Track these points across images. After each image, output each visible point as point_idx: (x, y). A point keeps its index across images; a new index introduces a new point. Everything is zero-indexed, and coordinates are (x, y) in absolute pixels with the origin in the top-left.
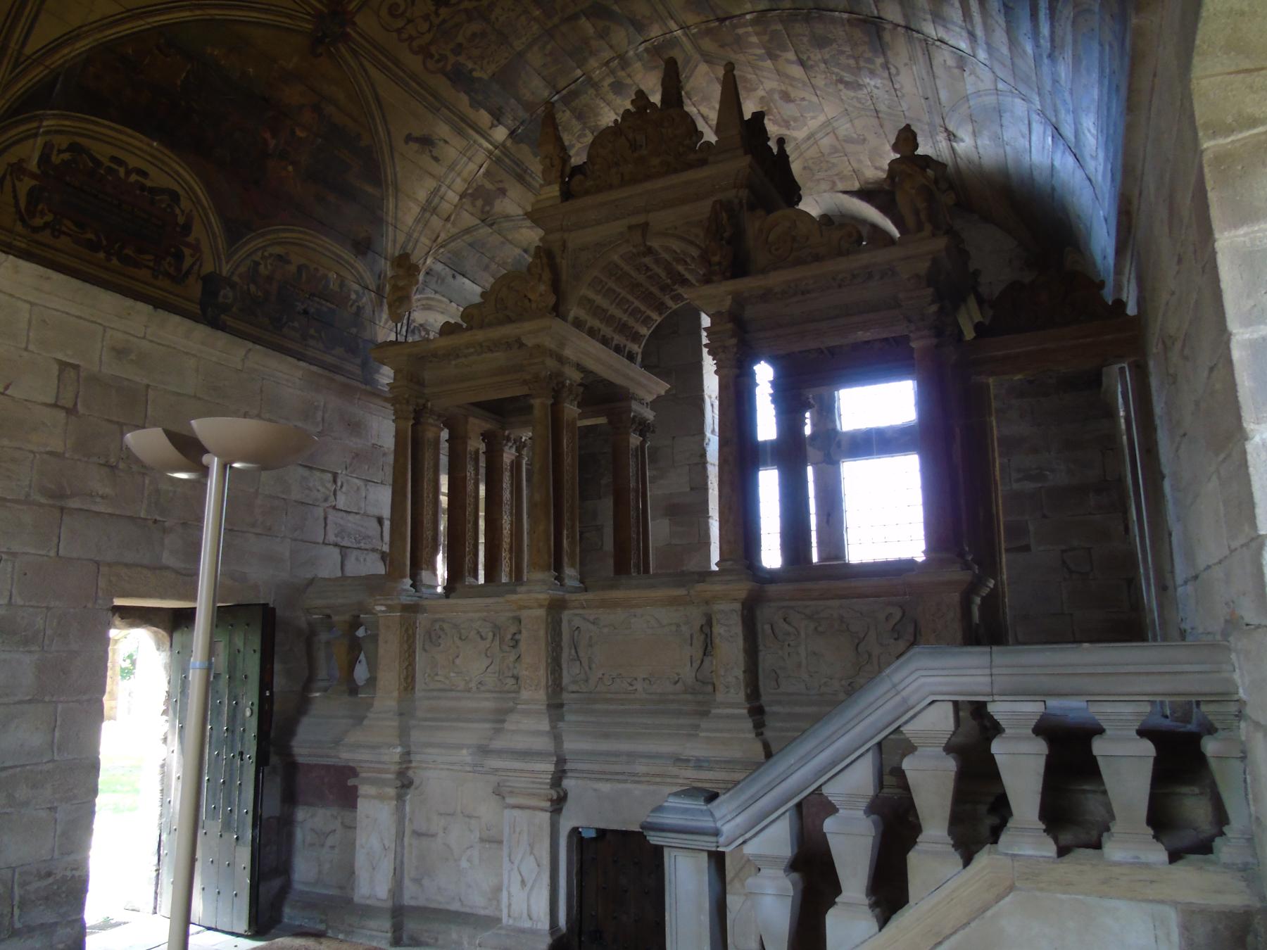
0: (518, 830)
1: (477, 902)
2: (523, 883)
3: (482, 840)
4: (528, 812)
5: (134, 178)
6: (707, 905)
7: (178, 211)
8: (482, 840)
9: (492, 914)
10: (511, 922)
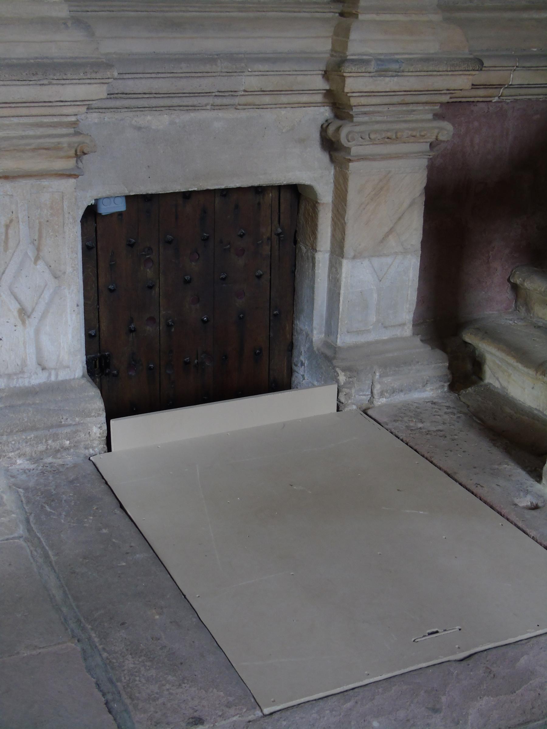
2: (24, 314)
4: (26, 184)
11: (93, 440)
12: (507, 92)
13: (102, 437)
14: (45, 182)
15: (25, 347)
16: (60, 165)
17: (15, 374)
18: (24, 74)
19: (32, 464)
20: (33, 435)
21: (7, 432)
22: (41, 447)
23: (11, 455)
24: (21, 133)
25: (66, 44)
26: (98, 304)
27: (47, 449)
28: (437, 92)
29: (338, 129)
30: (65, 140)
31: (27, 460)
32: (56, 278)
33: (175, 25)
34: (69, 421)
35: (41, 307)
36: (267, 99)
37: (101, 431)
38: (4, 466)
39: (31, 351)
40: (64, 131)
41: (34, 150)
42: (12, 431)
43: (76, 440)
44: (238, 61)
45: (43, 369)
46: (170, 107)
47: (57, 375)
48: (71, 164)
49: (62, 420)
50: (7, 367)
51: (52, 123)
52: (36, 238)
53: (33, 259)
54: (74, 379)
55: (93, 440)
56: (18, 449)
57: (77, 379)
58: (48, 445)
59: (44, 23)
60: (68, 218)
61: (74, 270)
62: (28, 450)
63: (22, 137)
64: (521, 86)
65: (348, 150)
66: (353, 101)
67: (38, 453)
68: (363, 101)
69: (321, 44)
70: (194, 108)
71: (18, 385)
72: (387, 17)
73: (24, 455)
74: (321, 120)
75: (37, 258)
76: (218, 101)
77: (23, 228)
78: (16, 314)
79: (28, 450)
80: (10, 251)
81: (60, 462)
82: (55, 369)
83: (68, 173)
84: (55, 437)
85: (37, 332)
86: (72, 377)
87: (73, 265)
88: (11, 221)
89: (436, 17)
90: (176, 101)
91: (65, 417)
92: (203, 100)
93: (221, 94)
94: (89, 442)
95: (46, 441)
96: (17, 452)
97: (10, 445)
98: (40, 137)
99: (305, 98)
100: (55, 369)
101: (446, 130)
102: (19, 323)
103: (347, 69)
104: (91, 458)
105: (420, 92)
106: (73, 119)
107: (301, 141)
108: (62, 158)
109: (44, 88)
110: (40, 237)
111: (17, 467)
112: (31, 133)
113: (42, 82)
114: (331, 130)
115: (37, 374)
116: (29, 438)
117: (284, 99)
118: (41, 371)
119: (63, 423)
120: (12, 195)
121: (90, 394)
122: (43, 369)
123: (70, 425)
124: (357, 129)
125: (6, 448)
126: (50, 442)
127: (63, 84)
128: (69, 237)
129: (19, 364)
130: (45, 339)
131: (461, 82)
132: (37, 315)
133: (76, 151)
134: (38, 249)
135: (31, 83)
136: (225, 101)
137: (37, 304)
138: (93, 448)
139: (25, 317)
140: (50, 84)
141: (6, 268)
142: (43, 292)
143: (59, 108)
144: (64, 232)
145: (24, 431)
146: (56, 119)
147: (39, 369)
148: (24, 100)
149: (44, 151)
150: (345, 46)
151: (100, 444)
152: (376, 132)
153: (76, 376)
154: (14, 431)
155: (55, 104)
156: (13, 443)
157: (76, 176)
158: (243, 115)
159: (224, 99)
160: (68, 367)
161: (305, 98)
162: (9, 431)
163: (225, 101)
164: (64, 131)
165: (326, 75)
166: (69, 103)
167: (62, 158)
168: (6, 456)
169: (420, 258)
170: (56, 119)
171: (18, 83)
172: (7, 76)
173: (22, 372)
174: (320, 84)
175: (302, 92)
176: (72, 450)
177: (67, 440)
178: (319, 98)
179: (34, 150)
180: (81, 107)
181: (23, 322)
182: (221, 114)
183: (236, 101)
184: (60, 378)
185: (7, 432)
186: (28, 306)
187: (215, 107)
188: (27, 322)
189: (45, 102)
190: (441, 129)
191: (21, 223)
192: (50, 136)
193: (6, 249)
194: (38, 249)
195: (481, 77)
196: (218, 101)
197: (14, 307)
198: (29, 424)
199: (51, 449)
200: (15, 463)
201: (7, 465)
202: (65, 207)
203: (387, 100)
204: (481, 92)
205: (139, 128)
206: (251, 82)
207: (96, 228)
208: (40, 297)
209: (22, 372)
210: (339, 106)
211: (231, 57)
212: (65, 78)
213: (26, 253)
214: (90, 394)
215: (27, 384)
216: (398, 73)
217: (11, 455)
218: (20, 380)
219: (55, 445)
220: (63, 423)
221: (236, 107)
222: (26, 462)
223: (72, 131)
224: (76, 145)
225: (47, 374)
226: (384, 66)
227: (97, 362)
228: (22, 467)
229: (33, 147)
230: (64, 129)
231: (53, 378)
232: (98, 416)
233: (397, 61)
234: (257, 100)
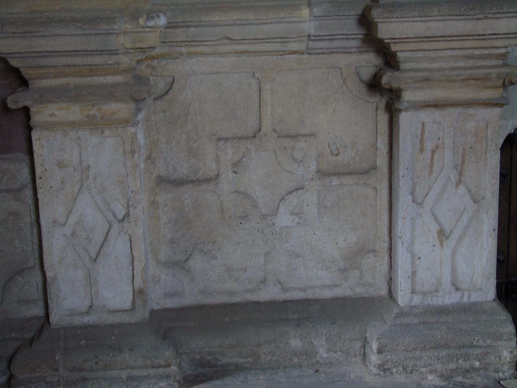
0: (429, 145)
1: (315, 277)
2: (442, 235)
3: (322, 174)
4: (455, 111)
6: (401, 140)
8: (322, 174)
9: (349, 293)
10: (417, 300)
11: (503, 364)
13: (513, 362)
14: (472, 111)
15: (441, 267)
16: (486, 94)
17: (430, 292)
18: (462, 9)
19: (442, 381)
20: (445, 353)
21: (420, 347)
22: (452, 366)
23: (423, 370)
24: (452, 64)
26: (509, 230)
27: (457, 368)
30: (494, 71)
31: (438, 377)
32: (475, 202)
34: (481, 343)
35: (459, 230)
37: (512, 356)
38: (416, 381)
39: (447, 271)
40: (493, 62)
42: (425, 347)
43: (486, 362)
45: (457, 289)
47: (469, 297)
48: (497, 93)
49: (474, 341)
50: (423, 285)
51: (483, 55)
52: (459, 163)
53: (455, 183)
54: (486, 302)
55: (503, 364)
56: (430, 365)
57: (489, 302)
58: (458, 364)
60: (491, 145)
61: (493, 195)
62: (439, 367)
63: (454, 69)
67: (448, 371)
71: (431, 303)
73: (435, 371)
75: (459, 183)
77: (448, 154)
78: (435, 234)
79: (439, 367)
80: (435, 175)
81: (470, 382)
82: (468, 290)
83: (494, 102)
84: (466, 357)
85: (454, 253)
86: (484, 300)
87: (493, 191)
88: (437, 147)
91: (476, 339)
94: (499, 366)
95: (457, 360)
96: (428, 368)
97: (423, 360)
98: (470, 68)
100: (468, 290)
102: (437, 243)
104: (501, 382)
106: (503, 51)
108: (489, 88)
109: (480, 22)
110: (463, 163)
111: (428, 383)
112: (462, 64)
113: (478, 16)
115: (451, 294)
116: (441, 355)
118: (454, 291)
119: (475, 344)
120: (440, 123)
121: (502, 317)
122: (457, 289)
123: (481, 347)
125: (418, 363)
126: (461, 361)
127: (498, 18)
128: (491, 164)
129: (435, 283)
130: (460, 262)
132: (455, 236)
133: (504, 81)
134: (460, 174)
135: (468, 17)
137: (455, 226)
138: (503, 373)
139: (444, 238)
140: (485, 18)
141: (429, 191)
142: (462, 215)
143: (491, 41)
144: (486, 159)
145: (437, 347)
146: (486, 52)
147: (453, 290)
148: (460, 34)
149: (473, 82)
151: (510, 369)
153: (488, 299)
154: (428, 347)
155: (487, 37)
156: (426, 358)
157: (501, 105)
160: (481, 289)
162: (422, 346)
164: (493, 62)
166: (501, 36)
167: (489, 88)
168: (418, 370)
169: (499, 155)
170: (486, 52)
171: (455, 17)
172: (446, 11)
173: (437, 291)
176: (482, 372)
177: (477, 361)
180: (512, 39)
181: (442, 243)
184: (472, 300)
185: (420, 347)
186: (447, 228)
188: (445, 243)
189: (479, 35)
191: (446, 149)
192: (479, 67)
193: (431, 173)
194: (460, 174)
197: (434, 228)
198: (442, 342)
199: (461, 368)
200: (426, 378)
201: (418, 380)
202: (489, 134)
207: (511, 157)
208: (459, 220)
209: (437, 291)
212: (501, 11)
213: (449, 177)
214: (502, 317)
215: (440, 303)
217: (423, 370)
218: (434, 299)
219: (466, 365)
220: (475, 344)
222: (437, 379)
223: (500, 62)
224: (504, 76)
225: (460, 295)
227: (504, 287)
228: (433, 383)
229: (463, 77)
230: (493, 61)
231: (465, 299)
232: (509, 340)
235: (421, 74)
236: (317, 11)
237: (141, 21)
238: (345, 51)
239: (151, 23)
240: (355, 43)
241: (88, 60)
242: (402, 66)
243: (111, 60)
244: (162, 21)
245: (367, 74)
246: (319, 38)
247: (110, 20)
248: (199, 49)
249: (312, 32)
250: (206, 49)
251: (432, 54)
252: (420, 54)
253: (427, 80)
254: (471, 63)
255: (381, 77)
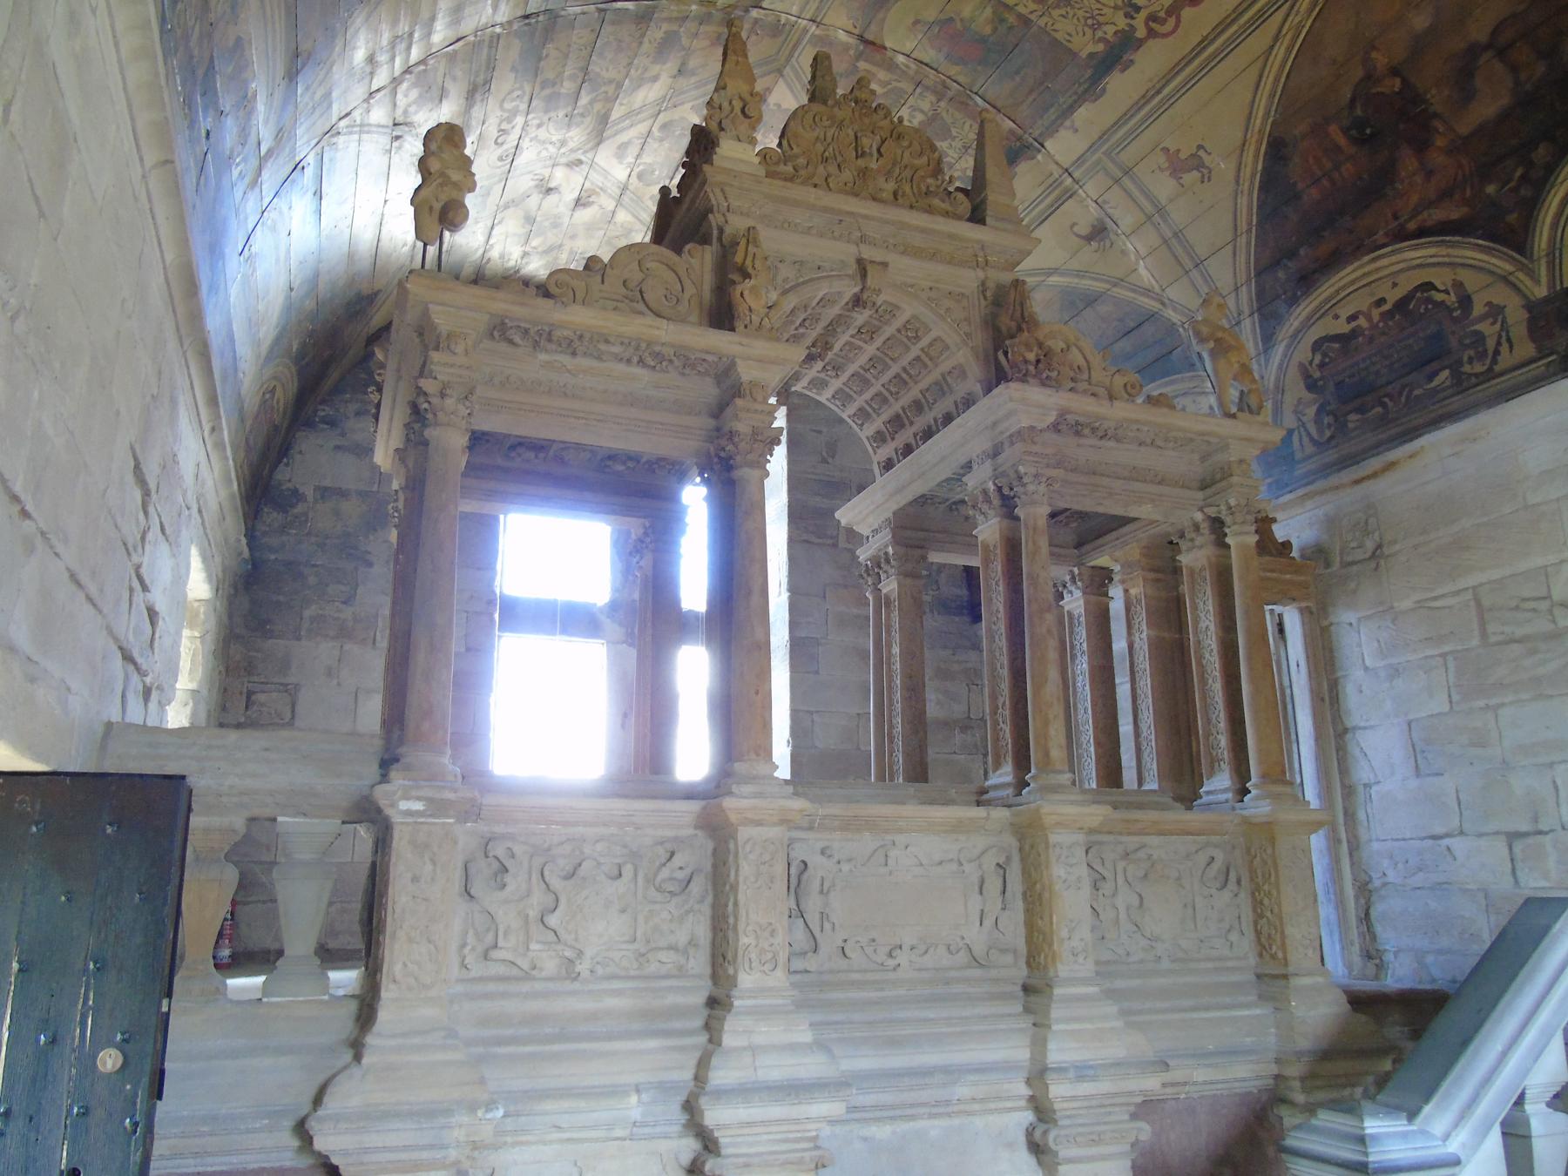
5: (1376, 314)
7: (1439, 297)
12: (1193, 1088)
25: (812, 1066)
28: (1131, 1093)
29: (1045, 1133)
30: (807, 1155)
33: (894, 1043)
36: (976, 1107)
41: (783, 1164)
44: (952, 1073)
46: (892, 1118)
59: (792, 1048)
64: (1205, 1083)
65: (1056, 1154)
66: (1056, 1106)
68: (1065, 1105)
69: (1020, 1053)
70: (912, 1118)
72: (1076, 1026)
74: (1025, 1124)
76: (935, 1110)
89: (1119, 1024)
90: (898, 1112)
92: (922, 1110)
93: (938, 1104)
99: (1009, 1104)
101: (1144, 1131)
103: (1050, 1077)
105: (1115, 1095)
107: (1010, 1145)
114: (1037, 1134)
117: (992, 1106)
124: (1063, 1132)
131: (1151, 1083)
136: (941, 1110)
150: (1044, 1054)
152: (1080, 1134)
158: (956, 1122)
159: (941, 1108)
161: (1009, 1104)
163: (941, 1110)
165: (1028, 1082)
174: (1025, 1091)
175: (1008, 1098)
178: (1023, 1103)
179: (783, 1164)
182: (936, 1122)
183: (950, 1109)
187: (932, 1116)
190: (1140, 1130)
195: (1168, 1077)
196: (935, 1110)
203: (1086, 1104)
204: (1169, 1090)
205: (865, 1139)
206: (962, 1091)
210: (1042, 1110)
211: (946, 1070)
216: (1094, 1079)
221: (949, 1115)
226: (1082, 1072)
233: (1091, 1067)
234: (967, 1107)
235: (741, 1160)
236: (645, 1097)
237: (480, 1113)
238: (666, 1137)
239: (489, 1116)
240: (676, 1128)
241: (415, 1155)
242: (723, 1152)
243: (439, 1155)
244: (500, 1113)
245: (686, 1159)
246: (644, 1124)
247: (448, 1112)
248: (524, 1138)
249: (639, 1118)
250: (530, 1138)
251: (750, 1139)
252: (739, 1139)
253: (747, 1165)
254: (784, 1147)
255: (704, 1163)
